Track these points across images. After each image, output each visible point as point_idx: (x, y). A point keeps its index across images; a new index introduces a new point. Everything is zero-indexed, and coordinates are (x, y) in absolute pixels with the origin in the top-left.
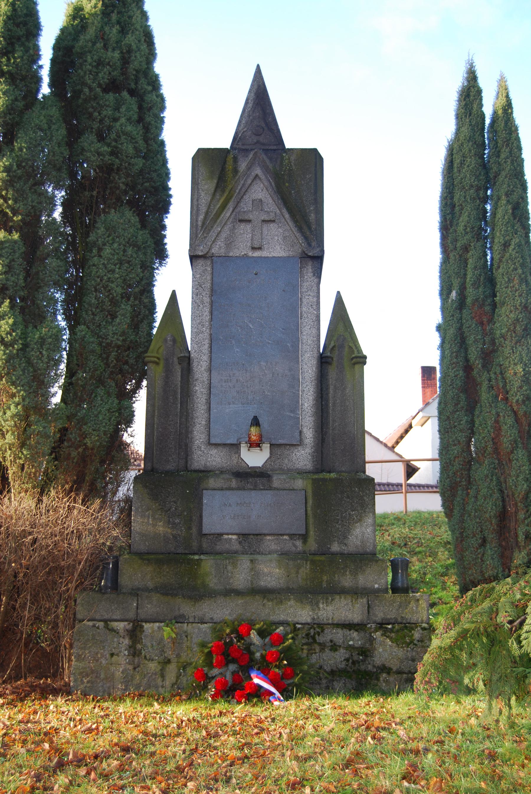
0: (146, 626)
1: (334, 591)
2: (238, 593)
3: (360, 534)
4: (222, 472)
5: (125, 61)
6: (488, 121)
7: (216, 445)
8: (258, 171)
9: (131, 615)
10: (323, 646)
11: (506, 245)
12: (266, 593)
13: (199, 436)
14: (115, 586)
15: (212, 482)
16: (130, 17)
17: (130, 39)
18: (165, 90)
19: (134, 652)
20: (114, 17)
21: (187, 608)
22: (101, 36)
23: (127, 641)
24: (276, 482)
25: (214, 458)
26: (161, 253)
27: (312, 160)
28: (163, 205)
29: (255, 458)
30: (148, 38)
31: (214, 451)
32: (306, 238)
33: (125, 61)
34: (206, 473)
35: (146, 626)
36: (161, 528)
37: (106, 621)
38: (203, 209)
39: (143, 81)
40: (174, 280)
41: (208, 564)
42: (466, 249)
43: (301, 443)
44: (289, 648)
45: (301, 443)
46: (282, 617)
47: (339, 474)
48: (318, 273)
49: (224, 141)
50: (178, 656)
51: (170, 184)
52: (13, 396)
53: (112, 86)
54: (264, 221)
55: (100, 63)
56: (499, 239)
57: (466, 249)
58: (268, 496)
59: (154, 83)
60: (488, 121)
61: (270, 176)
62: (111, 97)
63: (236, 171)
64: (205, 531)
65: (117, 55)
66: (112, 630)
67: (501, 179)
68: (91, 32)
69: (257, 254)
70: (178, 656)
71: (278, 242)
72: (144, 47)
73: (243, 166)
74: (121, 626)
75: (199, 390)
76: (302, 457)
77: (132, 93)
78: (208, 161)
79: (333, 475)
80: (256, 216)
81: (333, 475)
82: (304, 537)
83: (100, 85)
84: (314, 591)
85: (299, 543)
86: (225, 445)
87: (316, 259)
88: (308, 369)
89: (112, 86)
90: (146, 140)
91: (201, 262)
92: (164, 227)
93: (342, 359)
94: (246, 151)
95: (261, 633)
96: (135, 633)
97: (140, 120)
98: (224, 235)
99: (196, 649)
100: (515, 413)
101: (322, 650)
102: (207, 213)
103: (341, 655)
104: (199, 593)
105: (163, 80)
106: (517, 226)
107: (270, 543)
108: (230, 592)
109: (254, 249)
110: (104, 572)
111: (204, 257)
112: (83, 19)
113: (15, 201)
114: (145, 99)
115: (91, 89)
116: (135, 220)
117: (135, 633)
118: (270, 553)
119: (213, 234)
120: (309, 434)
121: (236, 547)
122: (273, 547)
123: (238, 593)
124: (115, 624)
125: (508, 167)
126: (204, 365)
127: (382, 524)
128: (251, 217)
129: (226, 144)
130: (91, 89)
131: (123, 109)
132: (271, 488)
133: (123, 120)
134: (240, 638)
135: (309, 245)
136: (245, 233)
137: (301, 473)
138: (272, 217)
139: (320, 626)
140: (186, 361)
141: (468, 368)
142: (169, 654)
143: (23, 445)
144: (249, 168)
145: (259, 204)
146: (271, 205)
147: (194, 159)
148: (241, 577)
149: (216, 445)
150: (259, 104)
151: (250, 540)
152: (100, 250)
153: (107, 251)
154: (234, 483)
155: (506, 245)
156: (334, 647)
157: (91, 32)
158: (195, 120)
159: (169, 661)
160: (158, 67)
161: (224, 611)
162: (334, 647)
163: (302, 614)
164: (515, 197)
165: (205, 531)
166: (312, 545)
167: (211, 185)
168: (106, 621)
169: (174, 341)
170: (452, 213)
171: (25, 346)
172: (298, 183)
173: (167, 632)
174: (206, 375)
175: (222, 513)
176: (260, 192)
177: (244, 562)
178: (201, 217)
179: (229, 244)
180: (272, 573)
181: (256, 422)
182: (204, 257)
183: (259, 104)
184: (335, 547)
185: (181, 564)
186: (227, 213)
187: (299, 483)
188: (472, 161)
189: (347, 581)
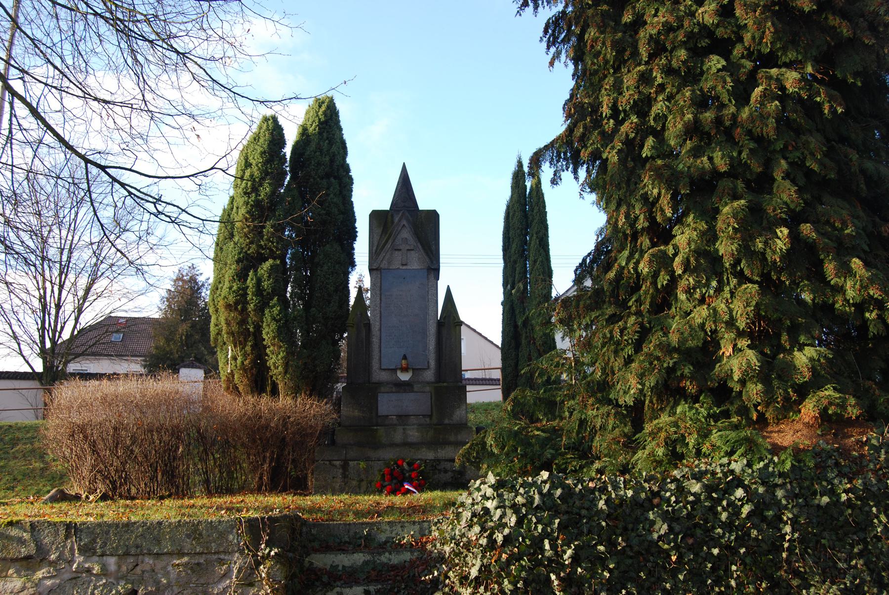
0: (351, 463)
1: (445, 443)
2: (397, 445)
3: (458, 414)
4: (388, 383)
5: (332, 161)
6: (528, 191)
7: (384, 370)
8: (404, 222)
9: (343, 458)
10: (440, 471)
11: (535, 261)
12: (411, 445)
13: (375, 365)
14: (333, 443)
15: (382, 389)
16: (334, 135)
17: (334, 149)
18: (353, 173)
19: (345, 476)
20: (325, 134)
21: (371, 454)
22: (319, 148)
23: (341, 471)
24: (416, 387)
25: (384, 376)
26: (353, 264)
27: (433, 217)
28: (352, 235)
29: (405, 377)
30: (343, 144)
31: (383, 373)
32: (430, 258)
33: (332, 161)
34: (380, 384)
35: (351, 463)
36: (356, 413)
37: (330, 461)
38: (376, 244)
39: (341, 170)
40: (360, 276)
41: (381, 431)
42: (515, 262)
43: (428, 368)
44: (423, 470)
45: (428, 368)
46: (419, 457)
47: (450, 380)
48: (437, 278)
49: (386, 206)
50: (367, 477)
51: (357, 225)
52: (281, 347)
53: (327, 176)
54: (408, 250)
55: (319, 164)
56: (532, 258)
57: (515, 262)
58: (412, 396)
59: (347, 169)
60: (528, 191)
61: (411, 228)
62: (325, 182)
63: (393, 222)
64: (380, 414)
65: (327, 159)
66: (333, 465)
67: (534, 224)
68: (313, 146)
69: (404, 267)
70: (367, 477)
71: (416, 262)
72: (341, 151)
73: (396, 220)
74: (337, 463)
75: (375, 340)
76: (429, 375)
77: (335, 178)
78: (376, 217)
79: (445, 384)
80: (404, 247)
81: (445, 384)
82: (430, 416)
83: (319, 177)
84: (436, 443)
85: (428, 420)
86: (389, 369)
87: (436, 271)
88: (432, 329)
89: (327, 176)
90: (344, 204)
91: (375, 272)
92: (353, 249)
93: (450, 322)
94: (399, 211)
95: (409, 464)
96: (345, 467)
97: (341, 192)
98: (387, 257)
99: (376, 473)
100: (539, 350)
101: (440, 473)
102: (377, 246)
103: (450, 474)
104: (377, 445)
105: (352, 167)
106: (542, 250)
107: (413, 420)
108: (393, 445)
109: (403, 265)
110: (328, 435)
111: (377, 269)
112: (308, 136)
113: (277, 243)
114: (340, 179)
115: (314, 179)
116: (339, 248)
117: (345, 467)
118: (413, 425)
119: (381, 257)
120: (433, 363)
121: (395, 422)
122: (415, 422)
123: (397, 445)
124: (335, 462)
125: (537, 218)
126: (377, 327)
127: (474, 408)
128: (401, 247)
129: (388, 208)
130: (314, 179)
131: (331, 189)
132: (413, 392)
133: (332, 195)
134: (398, 466)
135: (432, 262)
136: (398, 257)
137: (428, 383)
138: (412, 247)
139: (438, 461)
140: (368, 326)
141: (516, 326)
142: (363, 476)
143: (286, 372)
144: (400, 221)
145: (405, 240)
146: (412, 241)
147: (370, 215)
148: (398, 437)
149: (384, 370)
150: (405, 186)
151: (403, 418)
152: (322, 267)
153: (326, 267)
154: (394, 390)
155: (535, 261)
156: (446, 471)
157: (313, 146)
158: (370, 195)
159: (363, 480)
160: (349, 160)
161: (389, 454)
162: (446, 471)
163: (430, 455)
164: (541, 234)
165: (380, 414)
166: (435, 420)
167: (379, 231)
168: (330, 461)
169: (361, 314)
170: (509, 242)
171: (287, 321)
172: (426, 227)
173: (362, 465)
174: (378, 333)
175: (387, 404)
176: (406, 234)
177: (400, 429)
178: (375, 248)
179: (389, 263)
180: (414, 435)
181: (405, 357)
182: (377, 269)
183: (405, 186)
184: (446, 421)
185: (367, 431)
186: (388, 246)
187: (428, 389)
188: (518, 214)
189: (452, 438)
